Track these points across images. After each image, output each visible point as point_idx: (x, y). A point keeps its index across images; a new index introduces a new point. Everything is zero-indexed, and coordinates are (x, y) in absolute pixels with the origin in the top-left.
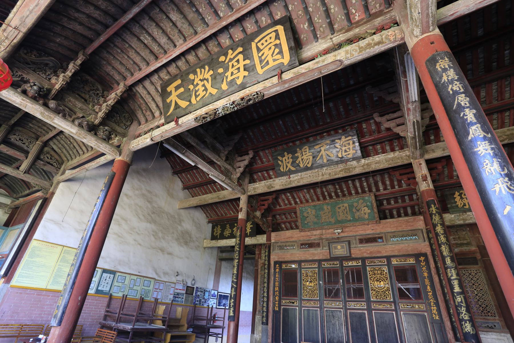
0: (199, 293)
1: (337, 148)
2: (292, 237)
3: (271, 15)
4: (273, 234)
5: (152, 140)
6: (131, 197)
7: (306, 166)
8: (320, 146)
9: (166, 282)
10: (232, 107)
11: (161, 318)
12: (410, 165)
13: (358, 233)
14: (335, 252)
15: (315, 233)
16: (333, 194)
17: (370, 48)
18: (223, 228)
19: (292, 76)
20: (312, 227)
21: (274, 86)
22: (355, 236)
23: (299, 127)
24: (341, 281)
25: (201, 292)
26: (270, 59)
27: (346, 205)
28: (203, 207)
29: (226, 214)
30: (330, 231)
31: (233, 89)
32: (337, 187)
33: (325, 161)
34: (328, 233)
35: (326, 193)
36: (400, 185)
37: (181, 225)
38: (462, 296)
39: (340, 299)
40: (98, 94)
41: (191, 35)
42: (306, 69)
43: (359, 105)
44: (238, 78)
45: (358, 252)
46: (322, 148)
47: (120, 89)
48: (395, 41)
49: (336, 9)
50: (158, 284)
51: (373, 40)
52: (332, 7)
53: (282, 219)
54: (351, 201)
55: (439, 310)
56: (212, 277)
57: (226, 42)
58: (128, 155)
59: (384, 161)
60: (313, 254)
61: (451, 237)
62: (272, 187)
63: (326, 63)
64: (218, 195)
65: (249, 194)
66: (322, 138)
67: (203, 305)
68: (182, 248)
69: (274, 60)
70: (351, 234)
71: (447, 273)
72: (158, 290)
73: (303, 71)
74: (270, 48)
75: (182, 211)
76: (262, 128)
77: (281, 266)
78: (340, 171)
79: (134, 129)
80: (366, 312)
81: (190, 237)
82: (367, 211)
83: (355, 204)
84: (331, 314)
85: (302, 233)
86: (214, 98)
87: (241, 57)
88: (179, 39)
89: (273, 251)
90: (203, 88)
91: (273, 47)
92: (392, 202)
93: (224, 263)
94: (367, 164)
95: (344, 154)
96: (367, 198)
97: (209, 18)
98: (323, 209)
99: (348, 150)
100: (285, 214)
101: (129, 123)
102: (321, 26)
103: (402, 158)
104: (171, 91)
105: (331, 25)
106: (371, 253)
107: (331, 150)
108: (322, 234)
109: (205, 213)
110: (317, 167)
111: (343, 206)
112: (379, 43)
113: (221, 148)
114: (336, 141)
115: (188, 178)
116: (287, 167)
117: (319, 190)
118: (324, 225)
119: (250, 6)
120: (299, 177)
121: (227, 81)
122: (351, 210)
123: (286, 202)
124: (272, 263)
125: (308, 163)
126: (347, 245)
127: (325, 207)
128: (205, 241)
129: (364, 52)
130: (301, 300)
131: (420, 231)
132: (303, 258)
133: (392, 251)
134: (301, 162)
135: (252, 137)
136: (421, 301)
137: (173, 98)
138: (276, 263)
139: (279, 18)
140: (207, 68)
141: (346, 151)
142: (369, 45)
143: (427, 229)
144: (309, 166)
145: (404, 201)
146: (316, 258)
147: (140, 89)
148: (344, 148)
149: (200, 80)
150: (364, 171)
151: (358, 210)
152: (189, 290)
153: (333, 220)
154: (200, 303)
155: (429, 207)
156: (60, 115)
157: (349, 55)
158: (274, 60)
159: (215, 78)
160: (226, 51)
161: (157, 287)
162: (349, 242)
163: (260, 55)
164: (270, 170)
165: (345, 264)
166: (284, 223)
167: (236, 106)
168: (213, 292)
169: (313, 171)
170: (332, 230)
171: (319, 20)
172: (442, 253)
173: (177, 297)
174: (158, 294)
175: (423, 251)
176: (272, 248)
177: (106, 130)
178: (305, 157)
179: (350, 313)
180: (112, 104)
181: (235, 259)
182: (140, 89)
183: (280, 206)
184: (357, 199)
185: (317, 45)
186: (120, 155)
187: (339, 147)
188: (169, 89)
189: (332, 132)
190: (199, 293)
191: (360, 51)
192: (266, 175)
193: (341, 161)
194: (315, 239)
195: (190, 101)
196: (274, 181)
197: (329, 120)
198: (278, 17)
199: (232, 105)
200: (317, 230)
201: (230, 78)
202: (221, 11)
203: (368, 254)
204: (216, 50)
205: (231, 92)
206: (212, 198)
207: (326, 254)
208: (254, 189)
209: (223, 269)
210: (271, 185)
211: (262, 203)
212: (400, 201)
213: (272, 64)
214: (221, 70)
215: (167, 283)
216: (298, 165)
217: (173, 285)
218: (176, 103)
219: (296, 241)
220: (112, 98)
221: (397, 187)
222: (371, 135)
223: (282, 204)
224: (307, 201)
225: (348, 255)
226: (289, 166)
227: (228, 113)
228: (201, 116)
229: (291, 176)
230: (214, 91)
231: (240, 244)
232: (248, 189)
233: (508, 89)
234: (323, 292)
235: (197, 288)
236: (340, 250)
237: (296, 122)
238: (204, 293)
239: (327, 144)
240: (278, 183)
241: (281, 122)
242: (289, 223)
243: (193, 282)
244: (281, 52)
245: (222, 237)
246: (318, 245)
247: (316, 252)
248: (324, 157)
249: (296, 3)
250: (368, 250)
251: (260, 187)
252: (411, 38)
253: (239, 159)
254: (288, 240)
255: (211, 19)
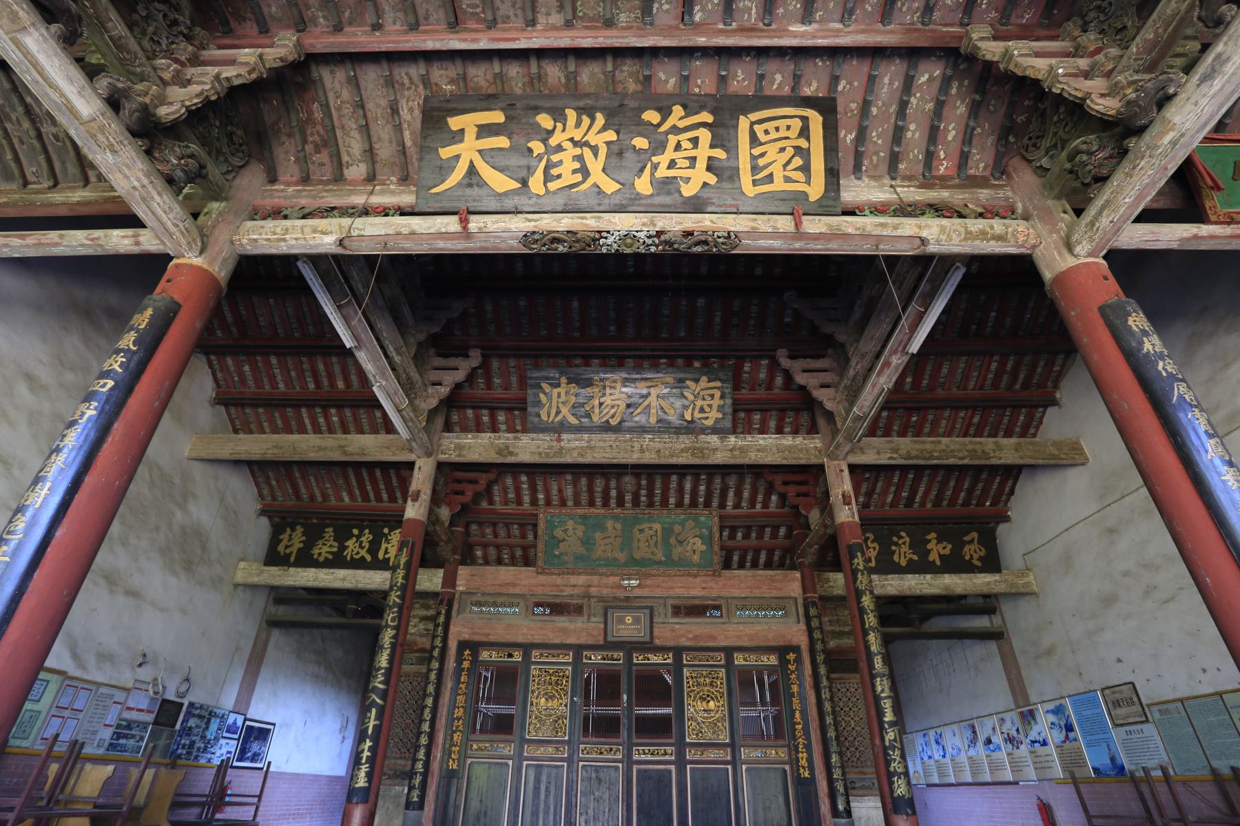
0: (192, 722)
1: (686, 398)
2: (514, 585)
3: (797, 78)
4: (463, 572)
5: (341, 243)
6: (44, 387)
7: (607, 421)
8: (650, 384)
9: (99, 685)
10: (649, 241)
11: (89, 808)
12: (821, 468)
13: (671, 593)
14: (618, 630)
15: (573, 580)
16: (628, 497)
17: (982, 240)
18: (313, 535)
19: (823, 230)
20: (570, 566)
21: (776, 235)
22: (665, 598)
23: (612, 328)
24: (625, 697)
25: (201, 717)
26: (777, 170)
27: (657, 526)
28: (257, 468)
29: (325, 497)
30: (612, 580)
31: (667, 200)
32: (644, 482)
33: (653, 420)
34: (603, 585)
35: (613, 493)
36: (765, 505)
37: (185, 509)
38: (896, 729)
39: (620, 740)
40: (175, 23)
41: (592, 19)
42: (857, 229)
43: (752, 322)
44: (688, 180)
45: (669, 634)
46: (653, 391)
47: (282, 48)
48: (1022, 246)
49: (917, 135)
50: (71, 691)
51: (992, 227)
52: (912, 127)
53: (483, 536)
54: (668, 520)
55: (810, 760)
56: (238, 675)
57: (667, 82)
58: (225, 260)
59: (774, 449)
60: (565, 631)
61: (827, 619)
62: (511, 454)
63: (899, 232)
64: (343, 443)
65: (443, 457)
66: (655, 367)
67: (196, 757)
68: (172, 580)
69: (788, 180)
70: (657, 592)
71: (873, 686)
72: (67, 713)
73: (850, 230)
74: (782, 150)
75: (198, 468)
76: (522, 303)
77: (475, 654)
78: (682, 451)
79: (250, 183)
80: (673, 767)
81: (204, 548)
82: (700, 546)
83: (677, 528)
84: (594, 775)
85: (543, 579)
86: (606, 201)
87: (705, 135)
88: (553, 11)
89: (458, 613)
90: (577, 165)
91: (790, 151)
92: (739, 535)
93: (276, 634)
94: (741, 449)
95: (697, 415)
96: (703, 519)
97: (666, 7)
98: (603, 529)
99: (707, 409)
100: (494, 524)
101: (237, 161)
102: (877, 153)
103: (807, 451)
104: (462, 131)
105: (894, 159)
106: (696, 637)
107: (672, 400)
108: (589, 586)
109: (257, 484)
110: (631, 430)
111: (651, 528)
112: (1000, 238)
113: (411, 322)
114: (688, 382)
115: (241, 374)
116: (558, 413)
117: (599, 484)
118: (600, 565)
119: (780, 37)
120: (584, 444)
121: (652, 174)
122: (665, 540)
123: (511, 496)
124: (453, 645)
125: (613, 417)
126: (648, 617)
127: (609, 524)
128: (242, 565)
129: (969, 242)
130: (524, 741)
131: (792, 602)
132: (538, 639)
133: (739, 637)
134: (597, 411)
135: (489, 316)
136: (780, 742)
137: (468, 150)
138: (463, 645)
139: (809, 93)
140: (600, 119)
141: (702, 410)
142: (983, 235)
143: (805, 599)
144: (613, 422)
145: (760, 536)
146: (571, 640)
147: (333, 81)
148: (699, 403)
149: (571, 140)
150: (732, 462)
151: (681, 543)
152: (167, 711)
153: (622, 557)
154: (189, 753)
155: (852, 557)
156: (54, 28)
157: (944, 237)
158: (788, 180)
159: (620, 154)
160: (666, 103)
161: (64, 702)
162: (651, 609)
163: (756, 152)
164: (502, 408)
165: (638, 659)
166: (485, 546)
167: (661, 243)
168: (232, 718)
169: (621, 437)
170: (616, 579)
171: (878, 137)
172: (867, 647)
173: (126, 736)
174: (63, 725)
175: (795, 641)
176: (455, 607)
177: (192, 156)
178: (608, 400)
179: (639, 771)
180: (236, 82)
181: (387, 626)
182: (333, 81)
183: (491, 502)
184: (682, 517)
185: (191, 99)
186: (201, 252)
187: (691, 397)
188: (455, 123)
189: (680, 362)
190: (192, 722)
191: (965, 239)
192: (486, 419)
193: (686, 428)
194: (572, 596)
195: (524, 183)
196: (515, 438)
197: (682, 334)
198: (808, 91)
199: (650, 237)
200: (579, 574)
201: (662, 172)
202: (703, 10)
203: (689, 639)
204: (632, 87)
205: (662, 206)
206: (320, 448)
207: (595, 633)
208: (459, 447)
209: (270, 650)
210: (507, 447)
211: (457, 487)
212: (754, 535)
213: (779, 185)
214: (641, 143)
215: (103, 690)
216: (588, 415)
217: (120, 696)
218: (472, 170)
219: (522, 596)
220: (243, 61)
221: (758, 506)
222: (753, 389)
223: (497, 499)
224: (563, 503)
225: (647, 639)
226: (565, 411)
227: (628, 251)
228: (550, 232)
229: (564, 436)
230: (610, 186)
231: (404, 588)
232: (440, 445)
233: (976, 374)
234: (579, 722)
235: (191, 705)
236: (628, 627)
237: (612, 314)
238: (208, 723)
239: (666, 384)
240: (528, 448)
241: (575, 304)
242: (498, 547)
243: (183, 688)
244: (806, 169)
245: (305, 559)
246: (578, 610)
247: (571, 626)
248: (653, 411)
249: (856, 84)
250: (689, 632)
251: (476, 446)
252: (1059, 253)
253: (439, 361)
254: (504, 590)
255: (667, 11)
